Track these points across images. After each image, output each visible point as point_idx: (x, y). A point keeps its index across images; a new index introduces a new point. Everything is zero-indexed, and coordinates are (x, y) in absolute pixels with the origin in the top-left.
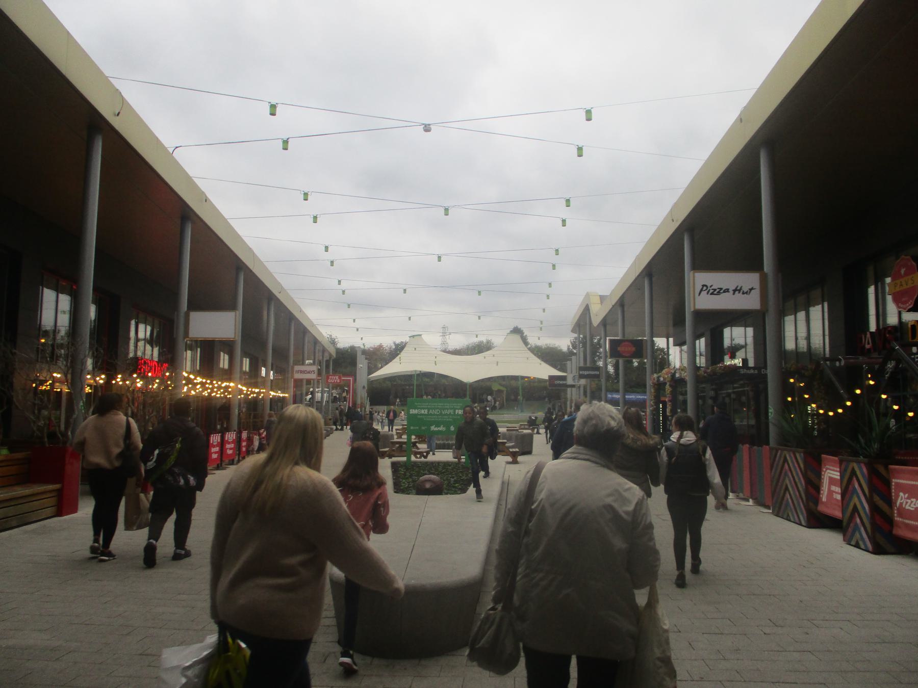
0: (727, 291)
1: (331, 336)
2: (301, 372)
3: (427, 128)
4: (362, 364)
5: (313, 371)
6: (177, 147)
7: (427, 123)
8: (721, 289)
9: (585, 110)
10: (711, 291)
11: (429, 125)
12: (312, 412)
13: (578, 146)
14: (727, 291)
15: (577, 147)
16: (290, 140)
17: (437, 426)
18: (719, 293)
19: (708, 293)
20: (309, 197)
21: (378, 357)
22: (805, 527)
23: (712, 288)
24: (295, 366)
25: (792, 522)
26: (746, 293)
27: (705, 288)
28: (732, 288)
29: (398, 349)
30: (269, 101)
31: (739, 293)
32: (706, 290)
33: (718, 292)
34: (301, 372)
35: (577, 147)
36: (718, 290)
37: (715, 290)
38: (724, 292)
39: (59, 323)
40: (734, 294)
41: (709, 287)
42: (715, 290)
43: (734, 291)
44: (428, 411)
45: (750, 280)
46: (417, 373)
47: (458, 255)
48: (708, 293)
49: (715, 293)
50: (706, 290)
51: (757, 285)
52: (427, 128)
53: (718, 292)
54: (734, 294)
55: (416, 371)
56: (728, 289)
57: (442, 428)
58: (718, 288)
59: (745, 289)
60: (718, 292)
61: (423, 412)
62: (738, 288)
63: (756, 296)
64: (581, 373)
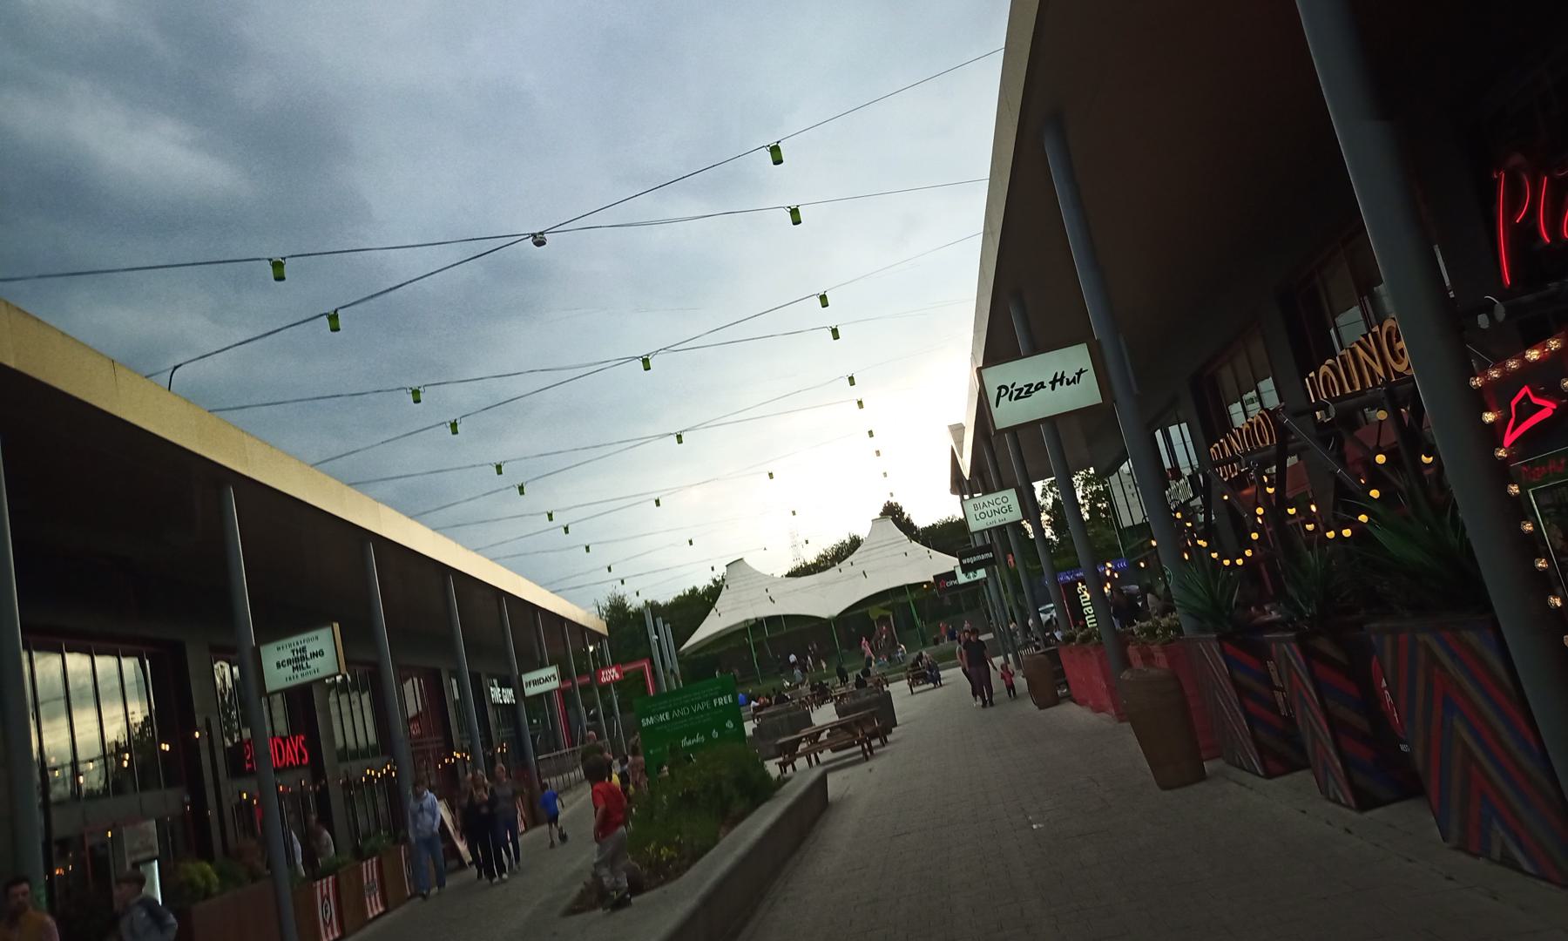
0: (1041, 385)
1: (625, 595)
2: (536, 682)
3: (539, 241)
4: (659, 635)
5: (554, 676)
6: (176, 368)
7: (537, 231)
8: (1031, 385)
9: (768, 148)
10: (1015, 393)
11: (542, 233)
13: (789, 207)
14: (1041, 385)
15: (789, 210)
16: (339, 312)
17: (691, 737)
18: (1028, 393)
19: (1010, 399)
20: (422, 396)
22: (1262, 777)
23: (1015, 388)
24: (523, 676)
25: (1246, 771)
26: (1074, 381)
27: (1003, 391)
28: (1048, 379)
29: (714, 592)
30: (270, 257)
31: (1061, 384)
32: (1006, 393)
33: (1029, 390)
34: (536, 682)
35: (789, 210)
36: (1025, 389)
37: (1021, 390)
38: (1036, 389)
39: (63, 722)
40: (1053, 388)
41: (1010, 387)
42: (1021, 390)
43: (1053, 383)
44: (671, 715)
45: (1075, 358)
46: (751, 623)
47: (632, 444)
48: (1010, 399)
49: (1023, 394)
50: (1006, 393)
51: (1087, 364)
52: (539, 241)
53: (1029, 390)
54: (1053, 388)
55: (747, 621)
56: (1042, 383)
57: (698, 739)
58: (1025, 386)
59: (1070, 375)
60: (1028, 392)
61: (662, 717)
62: (1059, 377)
63: (1090, 379)
64: (964, 562)
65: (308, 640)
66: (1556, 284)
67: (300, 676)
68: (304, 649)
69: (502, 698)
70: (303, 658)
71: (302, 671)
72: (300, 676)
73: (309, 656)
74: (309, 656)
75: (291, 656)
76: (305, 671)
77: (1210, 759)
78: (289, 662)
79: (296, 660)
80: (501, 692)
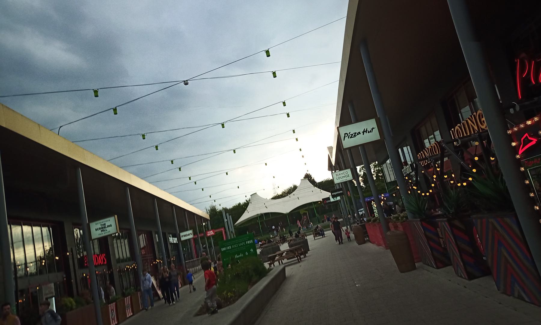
0: (359, 133)
1: (216, 206)
2: (185, 236)
3: (186, 83)
4: (227, 219)
5: (191, 233)
7: (185, 80)
8: (356, 133)
9: (265, 51)
10: (350, 136)
11: (187, 81)
12: (71, 303)
13: (272, 72)
14: (359, 133)
15: (272, 72)
16: (117, 108)
17: (238, 254)
18: (355, 136)
19: (349, 138)
20: (146, 137)
21: (241, 208)
23: (350, 134)
24: (180, 234)
26: (370, 131)
27: (346, 135)
28: (361, 131)
29: (246, 204)
30: (93, 89)
31: (366, 133)
32: (347, 136)
33: (355, 135)
34: (185, 236)
35: (272, 72)
36: (354, 134)
37: (352, 135)
38: (358, 134)
40: (363, 134)
41: (348, 134)
42: (352, 135)
43: (363, 132)
44: (231, 247)
45: (371, 124)
46: (259, 215)
47: (218, 153)
48: (349, 138)
49: (353, 136)
50: (347, 136)
51: (375, 126)
52: (186, 83)
53: (355, 135)
54: (363, 134)
55: (258, 214)
56: (360, 132)
57: (241, 255)
58: (354, 133)
59: (369, 130)
60: (355, 135)
61: (228, 248)
62: (365, 130)
63: (376, 131)
65: (106, 221)
66: (537, 98)
67: (103, 233)
68: (105, 224)
69: (173, 241)
70: (105, 227)
71: (104, 232)
72: (103, 233)
73: (106, 227)
74: (106, 227)
75: (100, 227)
76: (105, 232)
77: (417, 262)
78: (100, 229)
79: (102, 228)
80: (173, 239)
